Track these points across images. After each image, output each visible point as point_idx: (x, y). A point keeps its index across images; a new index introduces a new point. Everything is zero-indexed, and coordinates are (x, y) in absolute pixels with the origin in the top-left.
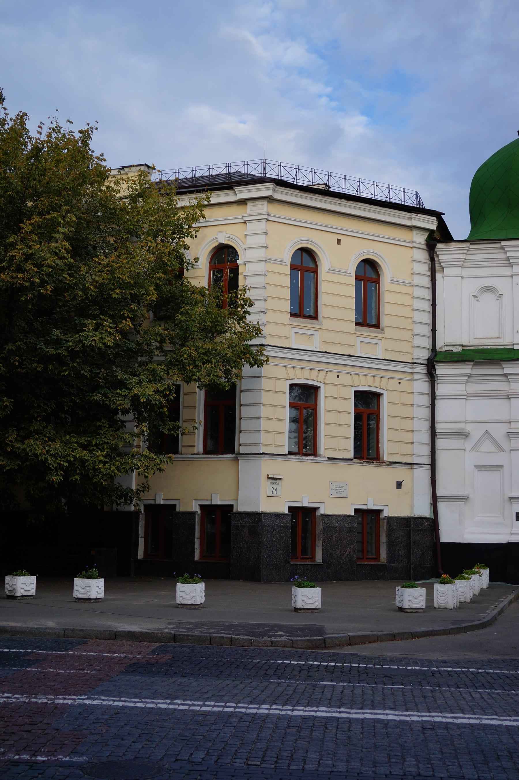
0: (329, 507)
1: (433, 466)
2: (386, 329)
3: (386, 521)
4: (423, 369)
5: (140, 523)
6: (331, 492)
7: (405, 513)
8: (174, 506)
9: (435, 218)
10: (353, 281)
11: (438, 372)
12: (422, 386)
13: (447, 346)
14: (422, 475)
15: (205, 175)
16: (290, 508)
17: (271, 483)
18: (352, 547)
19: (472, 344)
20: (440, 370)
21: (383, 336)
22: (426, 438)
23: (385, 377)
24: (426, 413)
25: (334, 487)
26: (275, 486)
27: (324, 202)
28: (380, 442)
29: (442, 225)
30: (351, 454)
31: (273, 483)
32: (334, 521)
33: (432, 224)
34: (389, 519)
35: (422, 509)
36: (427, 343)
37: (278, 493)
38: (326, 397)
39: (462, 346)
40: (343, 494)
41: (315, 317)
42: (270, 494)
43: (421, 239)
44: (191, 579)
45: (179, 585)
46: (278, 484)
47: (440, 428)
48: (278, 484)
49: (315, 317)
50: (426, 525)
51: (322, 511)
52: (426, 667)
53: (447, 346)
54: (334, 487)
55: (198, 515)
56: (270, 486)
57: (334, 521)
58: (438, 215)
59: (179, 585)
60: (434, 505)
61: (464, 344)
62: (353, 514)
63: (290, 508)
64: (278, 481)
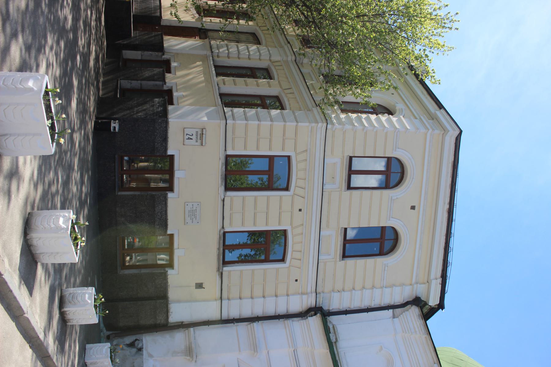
2: (343, 261)
3: (163, 271)
4: (309, 301)
5: (153, 53)
6: (190, 205)
7: (172, 294)
8: (172, 103)
9: (438, 303)
12: (297, 304)
13: (333, 327)
14: (211, 311)
16: (172, 157)
17: (197, 132)
19: (339, 350)
20: (315, 321)
21: (338, 257)
22: (247, 313)
24: (271, 312)
25: (194, 208)
26: (194, 137)
28: (240, 264)
29: (432, 311)
30: (229, 152)
31: (197, 136)
32: (160, 207)
33: (433, 301)
35: (177, 313)
36: (335, 306)
37: (187, 142)
38: (279, 224)
39: (335, 342)
41: (344, 256)
42: (187, 131)
43: (420, 291)
44: (99, 307)
45: (92, 290)
46: (197, 142)
48: (197, 142)
49: (344, 256)
50: (160, 320)
53: (333, 327)
54: (194, 208)
55: (163, 86)
56: (193, 132)
57: (160, 207)
58: (441, 306)
59: (92, 290)
61: (337, 343)
62: (169, 152)
63: (172, 157)
64: (199, 141)
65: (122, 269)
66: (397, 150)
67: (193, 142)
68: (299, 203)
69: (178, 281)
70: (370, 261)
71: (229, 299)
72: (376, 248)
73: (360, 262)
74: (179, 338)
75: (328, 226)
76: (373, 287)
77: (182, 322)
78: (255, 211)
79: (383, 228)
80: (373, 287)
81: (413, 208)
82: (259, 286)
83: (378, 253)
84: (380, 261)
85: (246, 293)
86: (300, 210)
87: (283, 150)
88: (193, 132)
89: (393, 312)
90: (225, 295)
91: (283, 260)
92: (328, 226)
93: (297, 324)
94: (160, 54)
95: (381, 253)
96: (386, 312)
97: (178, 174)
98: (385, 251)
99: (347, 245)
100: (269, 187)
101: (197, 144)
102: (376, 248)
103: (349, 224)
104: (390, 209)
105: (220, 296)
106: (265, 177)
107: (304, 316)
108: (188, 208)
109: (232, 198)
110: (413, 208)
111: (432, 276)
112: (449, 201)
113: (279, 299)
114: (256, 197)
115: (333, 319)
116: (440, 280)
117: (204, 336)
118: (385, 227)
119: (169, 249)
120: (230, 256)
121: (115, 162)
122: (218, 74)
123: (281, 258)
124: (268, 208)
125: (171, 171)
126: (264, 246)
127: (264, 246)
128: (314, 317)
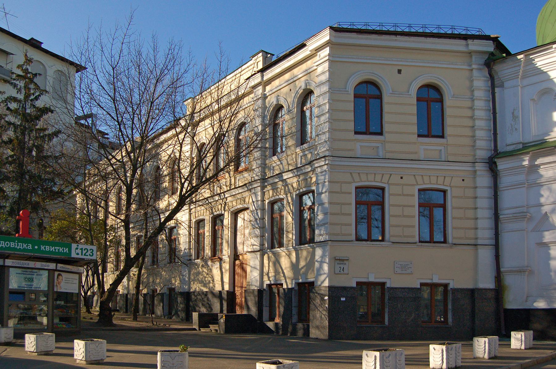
0: (395, 281)
1: (497, 246)
4: (481, 168)
9: (492, 42)
10: (415, 101)
11: (500, 167)
14: (486, 255)
15: (448, 32)
16: (358, 283)
18: (417, 313)
19: (531, 140)
20: (502, 165)
23: (426, 175)
25: (399, 266)
26: (342, 266)
27: (16, 40)
29: (500, 47)
31: (341, 264)
33: (490, 47)
34: (455, 290)
35: (487, 282)
37: (346, 271)
39: (523, 144)
40: (409, 271)
47: (504, 214)
50: (491, 295)
51: (388, 285)
52: (19, 225)
54: (399, 266)
56: (337, 267)
58: (495, 40)
60: (498, 278)
62: (355, 285)
63: (358, 283)
64: (345, 262)
65: (447, 324)
66: (347, 90)
67: (346, 267)
68: (395, 179)
69: (460, 281)
70: (448, 112)
71: (477, 239)
72: (435, 106)
73: (448, 121)
74: (509, 280)
75: (416, 153)
76: (472, 118)
77: (496, 277)
78: (402, 212)
79: (419, 100)
80: (472, 118)
81: (399, 71)
82: (467, 214)
83: (440, 104)
84: (448, 101)
85: (471, 224)
86: (402, 178)
87: (350, 193)
88: (337, 267)
89: (497, 87)
90: (472, 242)
91: (444, 192)
92: (416, 153)
93: (505, 181)
94: (264, 292)
95: (380, 97)
96: (497, 95)
97: (372, 279)
98: (378, 93)
99: (433, 134)
100: (382, 204)
101: (347, 264)
102: (435, 106)
103: (413, 134)
104: (402, 94)
105: (473, 246)
106: (374, 208)
107: (496, 173)
108: (399, 271)
109: (391, 236)
110: (399, 71)
111: (463, 49)
112: (388, 36)
113: (479, 216)
114: (391, 216)
115: (500, 149)
116: (470, 41)
117: (507, 263)
118: (417, 98)
119: (433, 286)
120: (438, 237)
121: (362, 327)
122: (189, 356)
123: (442, 193)
124: (399, 206)
125: (370, 285)
126: (432, 204)
127: (432, 204)
128: (498, 164)
